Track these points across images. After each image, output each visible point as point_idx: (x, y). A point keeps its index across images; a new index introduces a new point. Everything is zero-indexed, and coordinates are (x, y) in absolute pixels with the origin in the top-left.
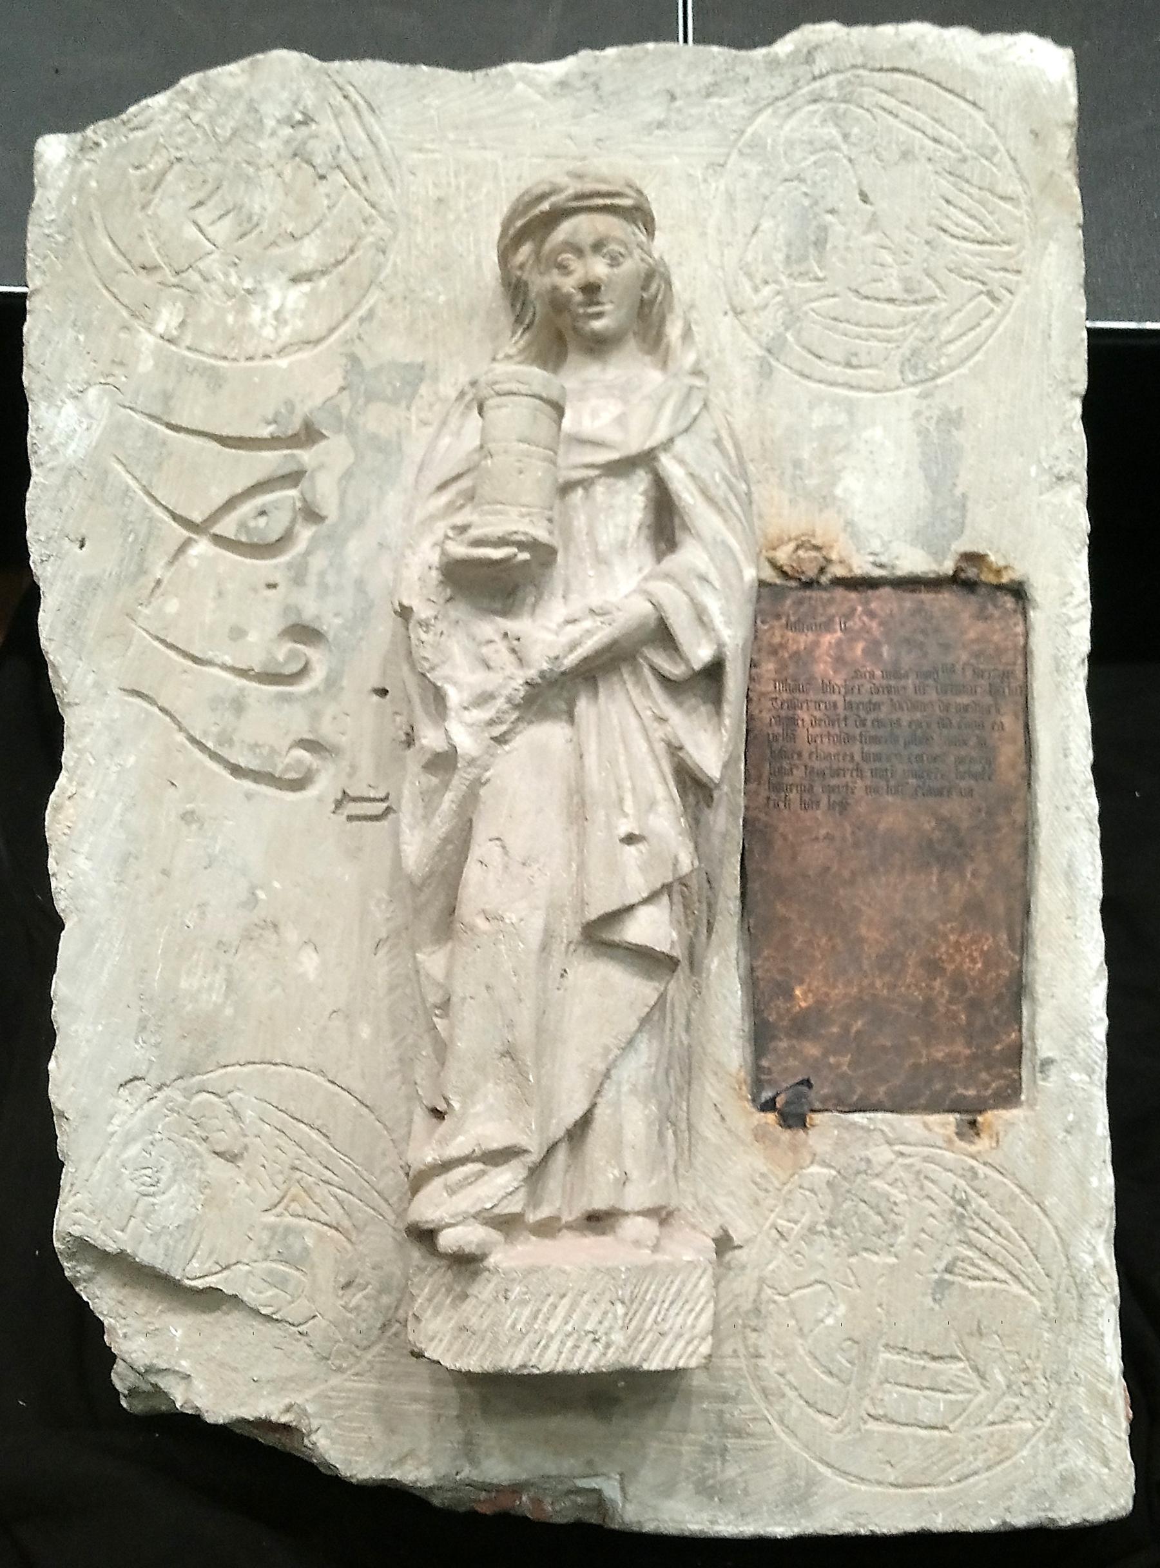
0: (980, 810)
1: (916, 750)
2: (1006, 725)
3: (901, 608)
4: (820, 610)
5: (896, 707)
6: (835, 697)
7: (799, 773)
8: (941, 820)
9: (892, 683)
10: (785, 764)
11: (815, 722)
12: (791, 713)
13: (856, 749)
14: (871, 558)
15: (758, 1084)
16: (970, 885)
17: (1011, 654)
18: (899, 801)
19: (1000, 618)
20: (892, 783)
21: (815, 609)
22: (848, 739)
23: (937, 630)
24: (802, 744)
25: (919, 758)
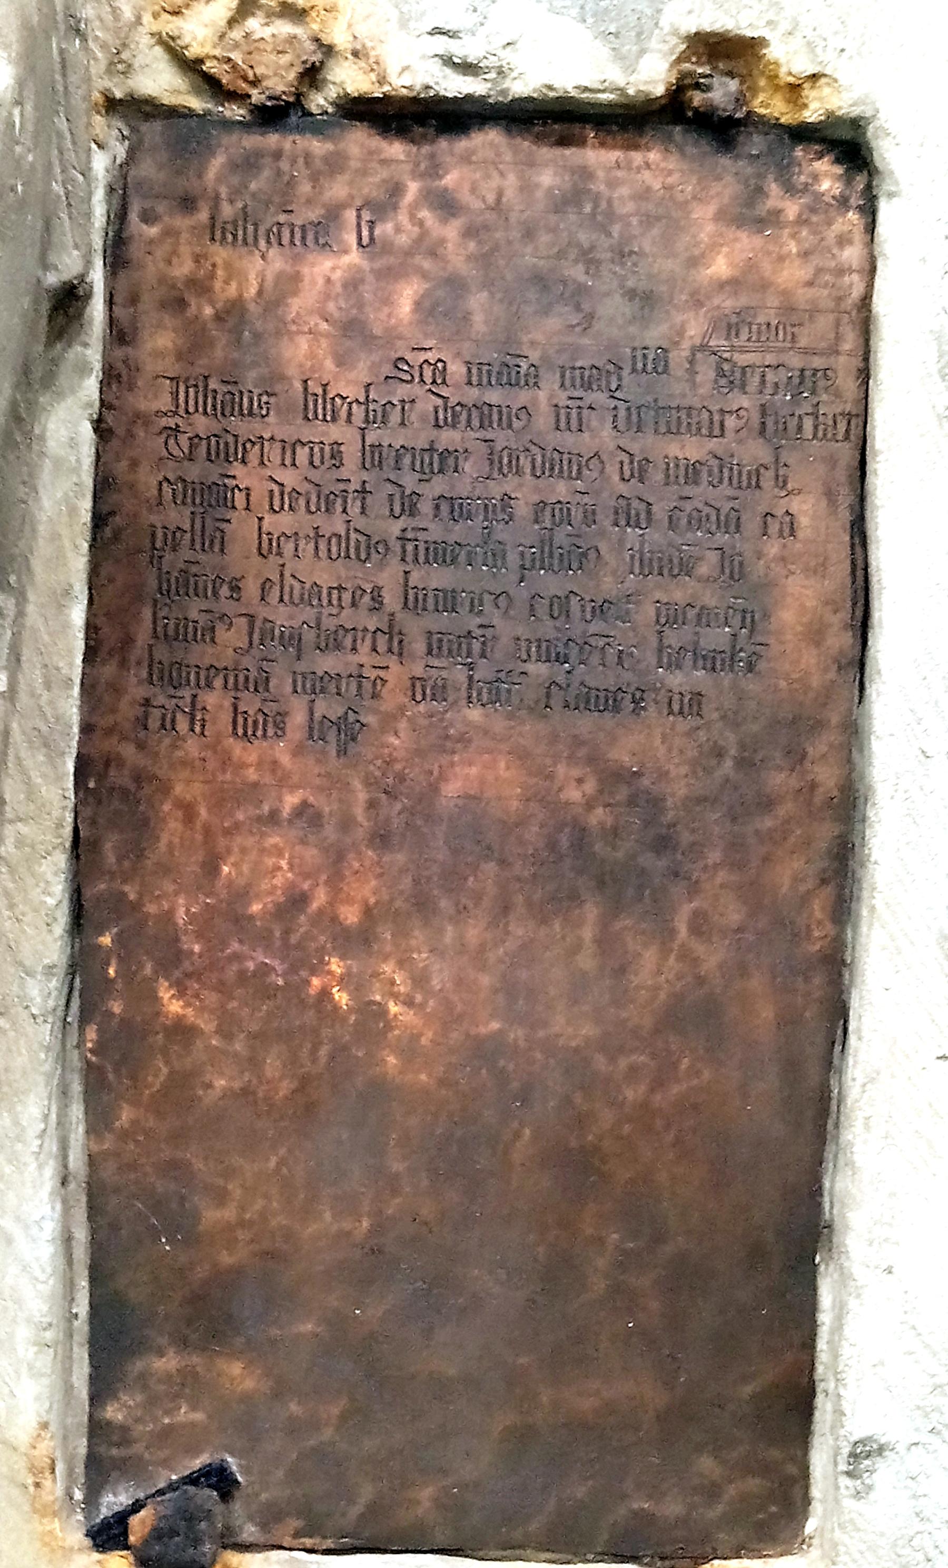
0: (719, 753)
1: (551, 584)
2: (804, 521)
3: (526, 188)
4: (305, 188)
5: (499, 463)
6: (335, 432)
7: (231, 637)
8: (613, 777)
9: (494, 396)
10: (194, 609)
11: (283, 500)
12: (213, 473)
13: (388, 577)
14: (442, 45)
15: (98, 1471)
16: (685, 955)
17: (824, 323)
18: (499, 725)
19: (801, 221)
20: (484, 671)
21: (291, 183)
22: (370, 548)
23: (622, 254)
24: (241, 556)
25: (560, 607)
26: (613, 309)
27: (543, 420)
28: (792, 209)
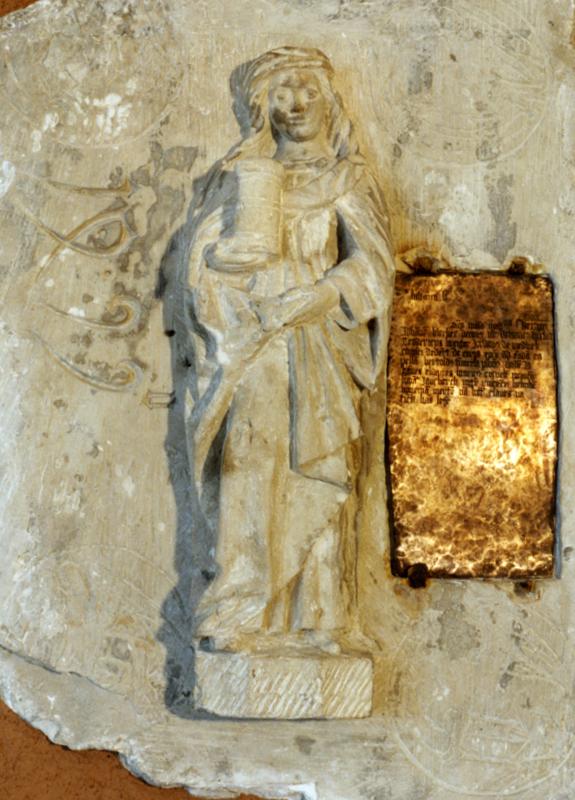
9: (474, 330)
12: (415, 347)
26: (499, 313)
27: (486, 335)
28: (536, 291)
